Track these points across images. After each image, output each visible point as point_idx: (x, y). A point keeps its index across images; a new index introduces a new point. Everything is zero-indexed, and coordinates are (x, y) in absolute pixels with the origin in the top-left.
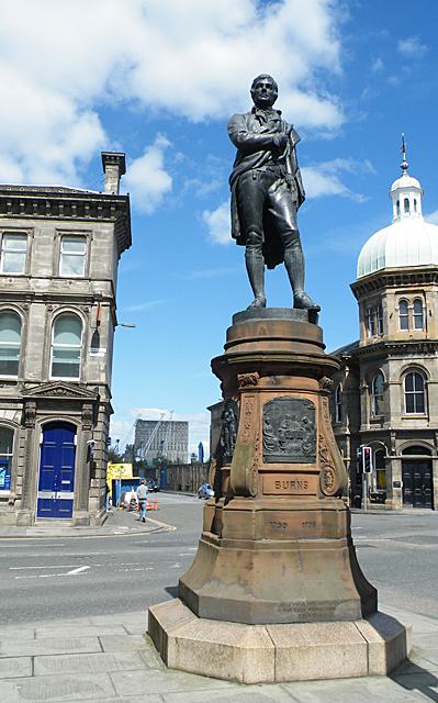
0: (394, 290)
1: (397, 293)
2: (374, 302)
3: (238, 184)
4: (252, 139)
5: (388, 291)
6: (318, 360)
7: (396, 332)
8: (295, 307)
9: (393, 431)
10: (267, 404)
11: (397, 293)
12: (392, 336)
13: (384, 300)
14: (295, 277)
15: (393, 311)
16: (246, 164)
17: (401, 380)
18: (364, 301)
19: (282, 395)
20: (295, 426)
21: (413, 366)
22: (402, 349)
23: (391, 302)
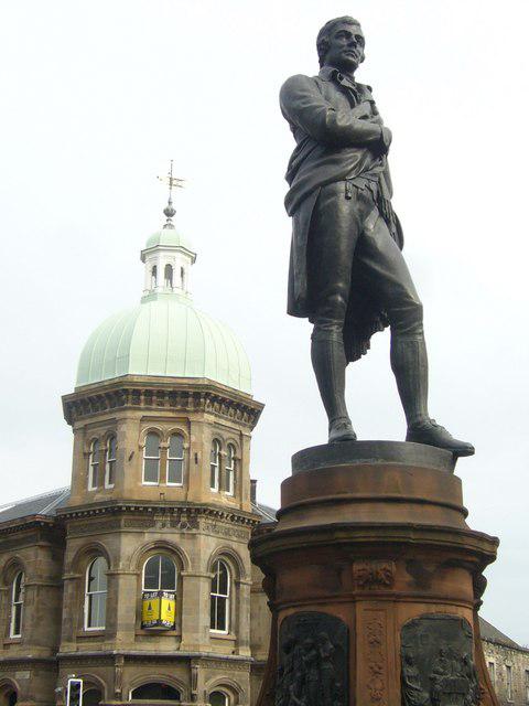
0: (141, 414)
1: (144, 419)
2: (102, 431)
3: (317, 204)
4: (350, 127)
5: (129, 414)
6: (436, 537)
7: (140, 485)
8: (410, 437)
9: (119, 655)
10: (408, 626)
11: (144, 419)
12: (131, 491)
13: (124, 428)
14: (410, 376)
15: (136, 449)
16: (309, 174)
17: (139, 567)
18: (86, 428)
19: (434, 609)
20: (454, 670)
21: (162, 546)
22: (144, 514)
23: (132, 433)
